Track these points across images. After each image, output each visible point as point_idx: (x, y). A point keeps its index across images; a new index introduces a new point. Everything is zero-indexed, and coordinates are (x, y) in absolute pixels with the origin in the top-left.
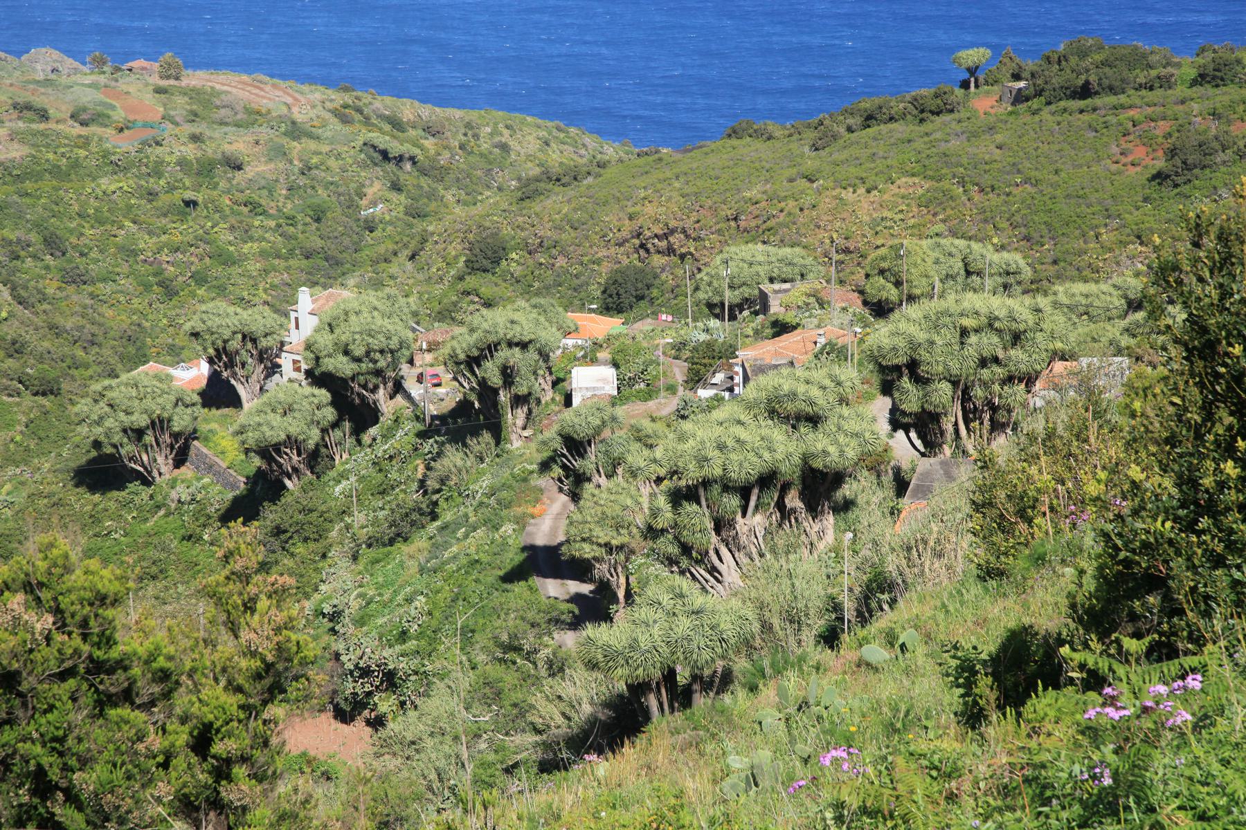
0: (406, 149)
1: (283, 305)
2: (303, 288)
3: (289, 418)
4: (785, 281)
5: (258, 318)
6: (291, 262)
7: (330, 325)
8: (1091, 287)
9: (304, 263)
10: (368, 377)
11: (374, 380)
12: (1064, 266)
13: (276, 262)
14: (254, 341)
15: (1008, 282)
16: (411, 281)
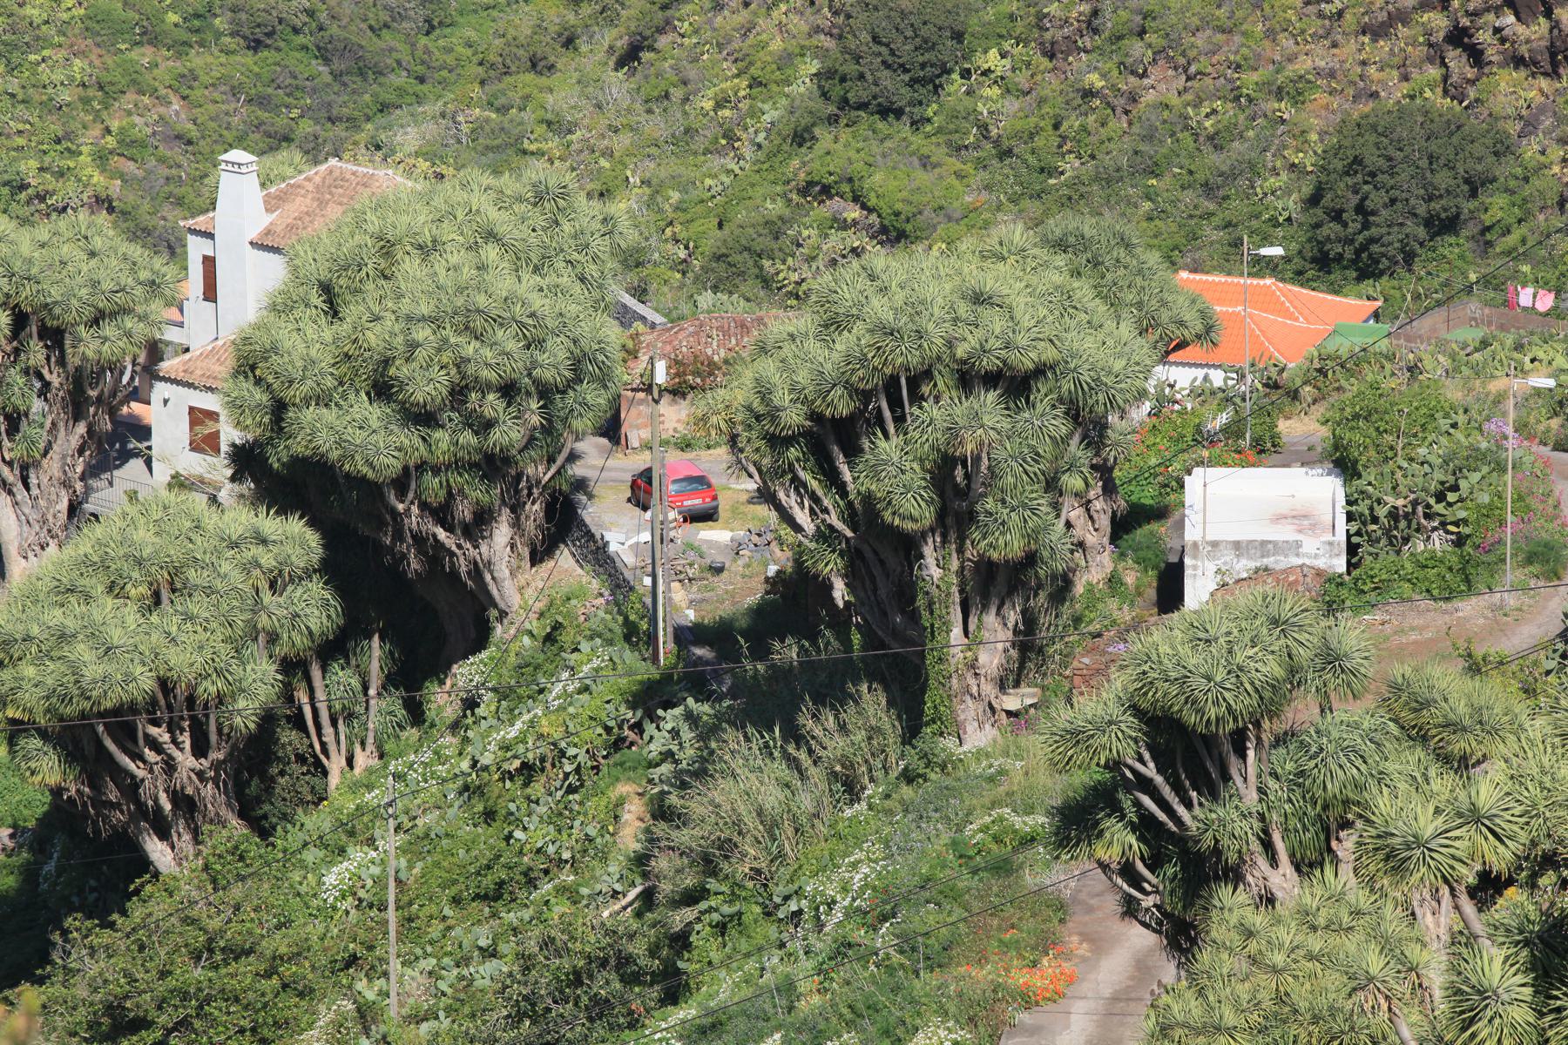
1: (159, 219)
2: (237, 155)
3: (168, 618)
6: (197, 59)
7: (326, 289)
10: (456, 479)
11: (475, 493)
13: (144, 56)
14: (54, 337)
16: (621, 143)
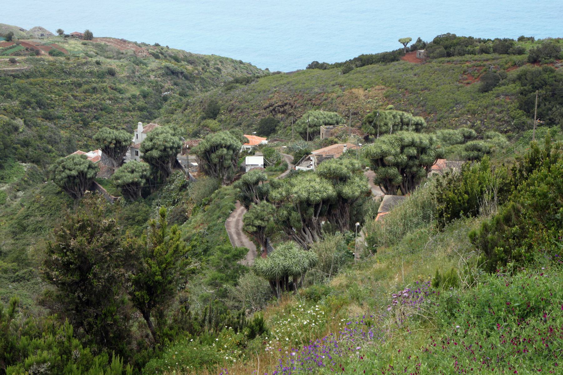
0: (180, 69)
1: (131, 130)
2: (140, 123)
4: (331, 125)
5: (122, 134)
8: (451, 131)
9: (139, 113)
12: (441, 123)
15: (418, 128)
